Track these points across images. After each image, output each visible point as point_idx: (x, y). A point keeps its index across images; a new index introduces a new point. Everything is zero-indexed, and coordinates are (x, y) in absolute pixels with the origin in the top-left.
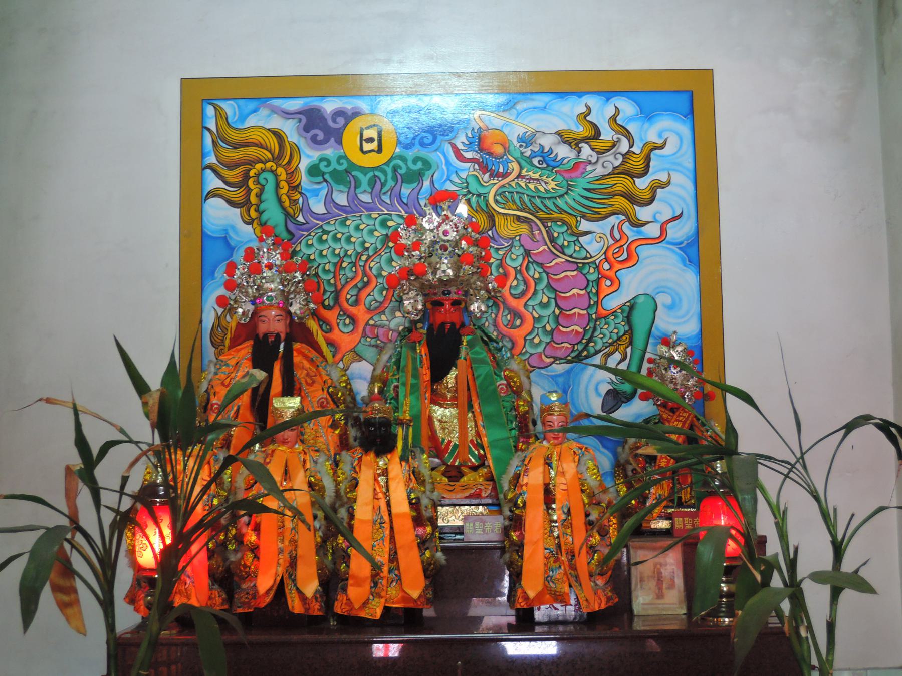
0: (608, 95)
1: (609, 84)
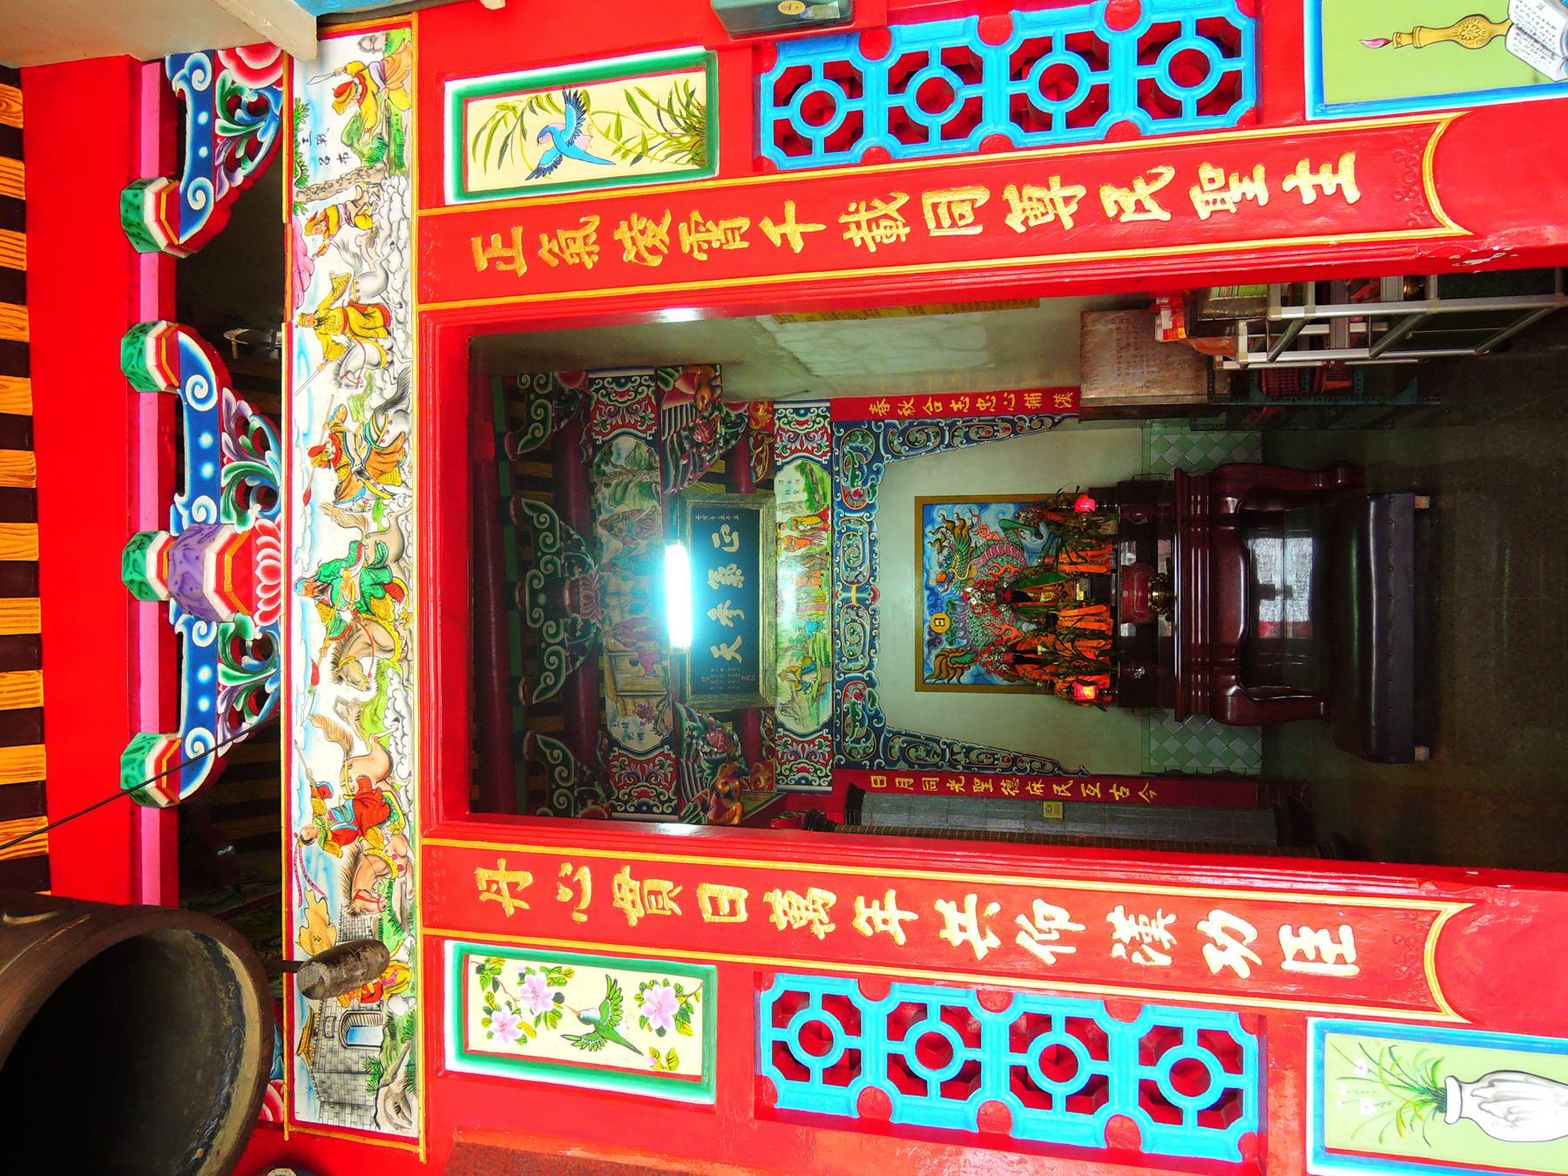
0: (924, 535)
1: (920, 535)
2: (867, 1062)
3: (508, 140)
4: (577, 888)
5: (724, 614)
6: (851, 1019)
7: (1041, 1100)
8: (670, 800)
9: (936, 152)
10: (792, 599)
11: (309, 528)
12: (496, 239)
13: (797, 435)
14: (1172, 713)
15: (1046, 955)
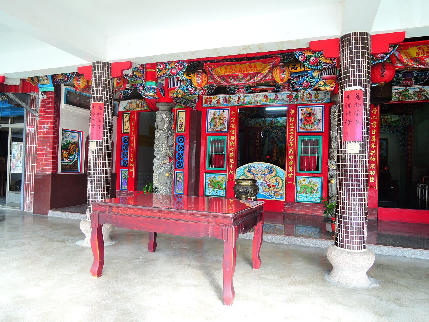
4: (374, 118)
11: (413, 89)
15: (371, 159)
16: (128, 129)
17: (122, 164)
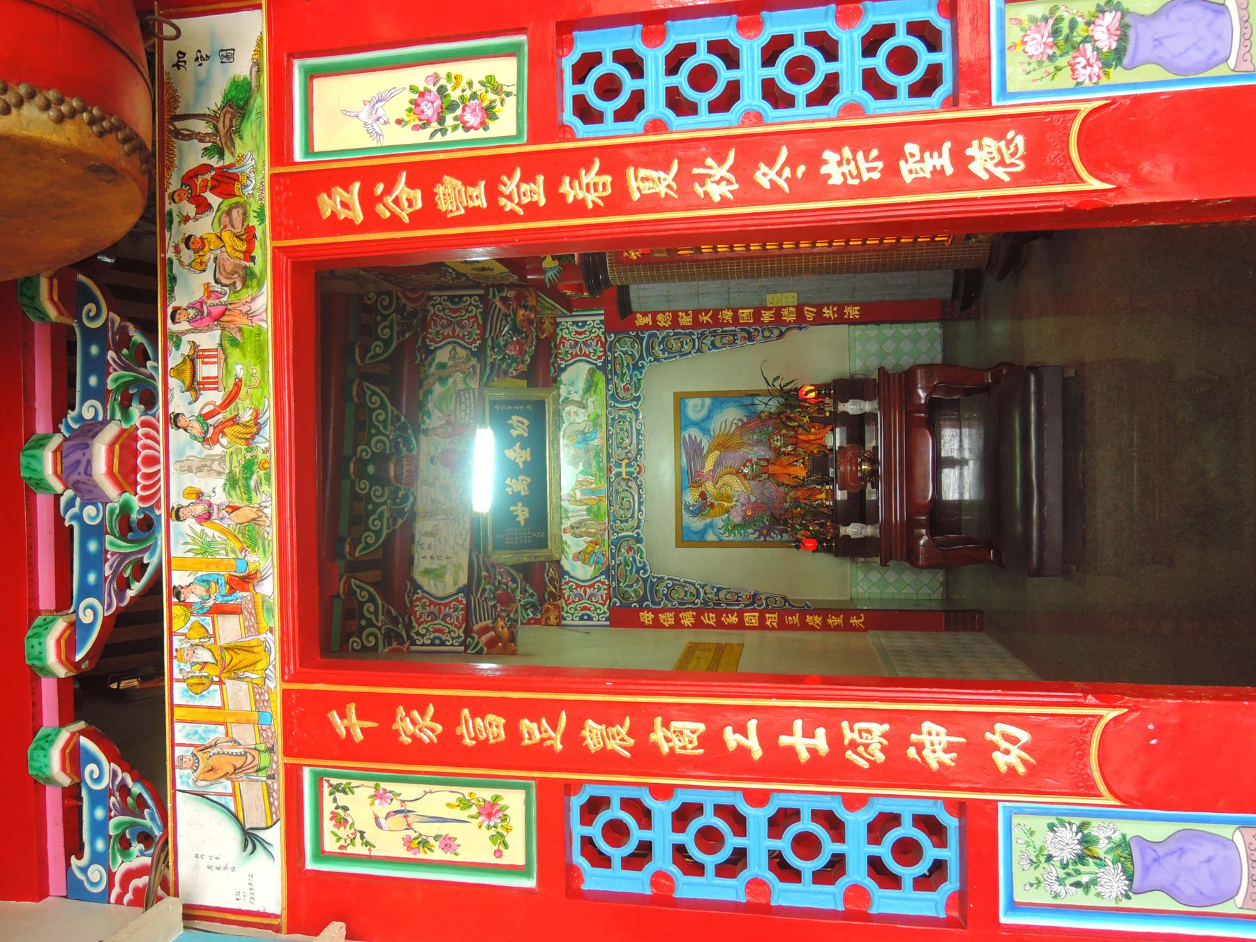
2: (752, 857)
3: (359, 110)
5: (521, 485)
6: (739, 824)
7: (697, 869)
8: (459, 637)
9: (705, 124)
10: (571, 474)
12: (935, 154)
13: (576, 343)
14: (878, 559)
16: (490, 811)
17: (932, 904)
